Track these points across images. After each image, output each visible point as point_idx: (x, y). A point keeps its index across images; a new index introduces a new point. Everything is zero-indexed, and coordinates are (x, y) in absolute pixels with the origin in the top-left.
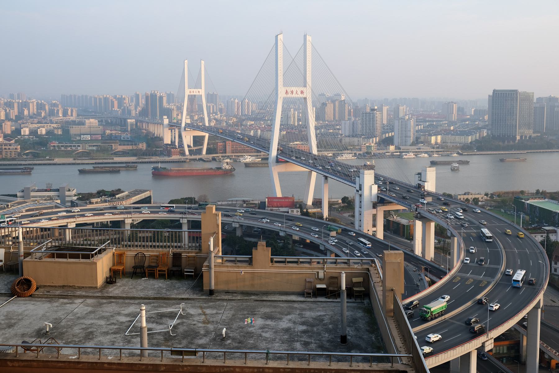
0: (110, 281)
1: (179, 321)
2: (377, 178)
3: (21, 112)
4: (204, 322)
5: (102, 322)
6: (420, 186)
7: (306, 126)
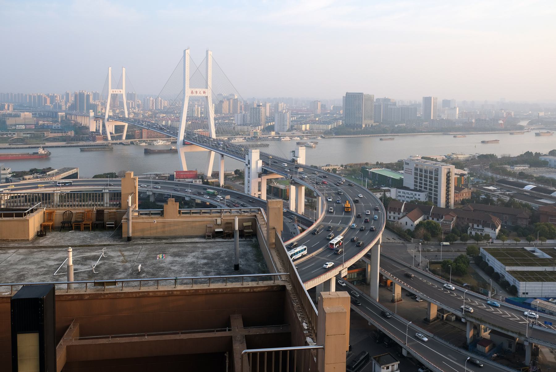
0: (41, 234)
1: (101, 262)
2: (263, 156)
4: (122, 262)
5: (33, 267)
6: (294, 161)
7: (207, 118)
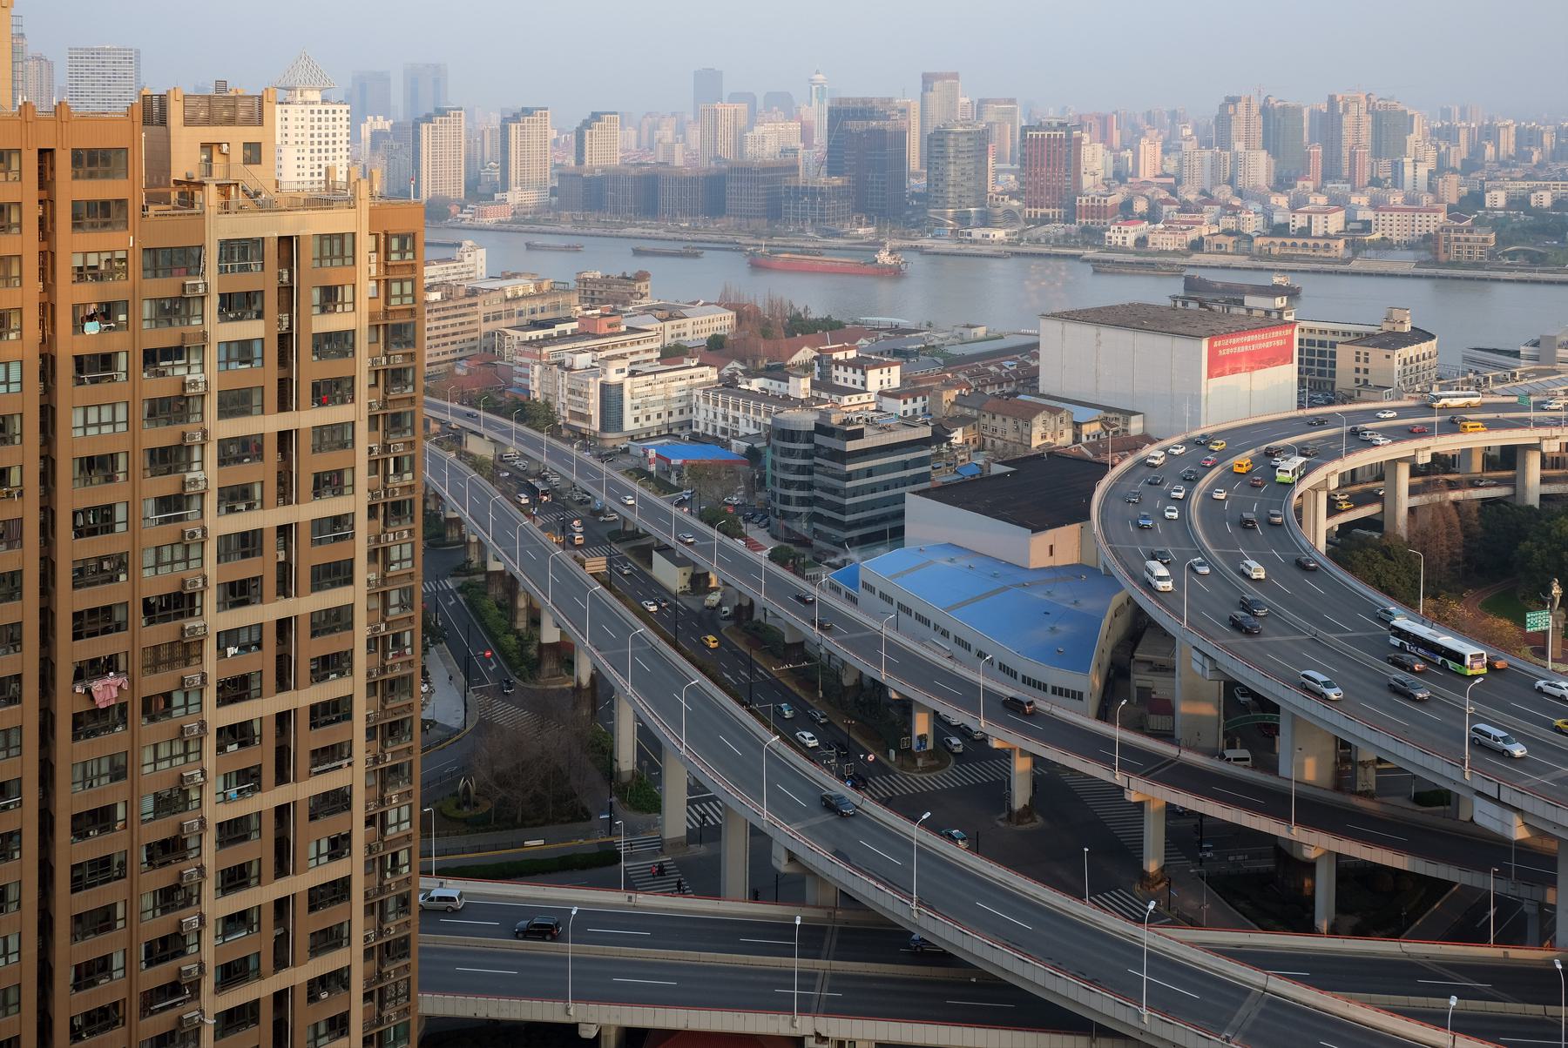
3: (1476, 151)
